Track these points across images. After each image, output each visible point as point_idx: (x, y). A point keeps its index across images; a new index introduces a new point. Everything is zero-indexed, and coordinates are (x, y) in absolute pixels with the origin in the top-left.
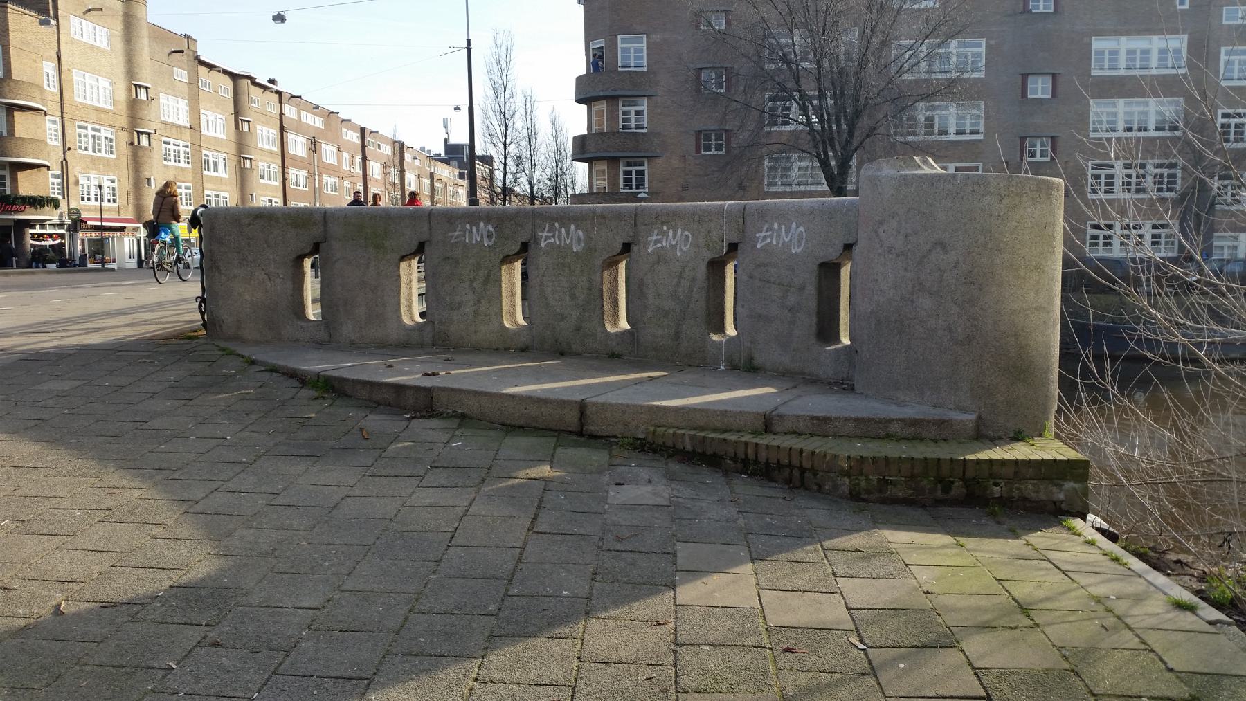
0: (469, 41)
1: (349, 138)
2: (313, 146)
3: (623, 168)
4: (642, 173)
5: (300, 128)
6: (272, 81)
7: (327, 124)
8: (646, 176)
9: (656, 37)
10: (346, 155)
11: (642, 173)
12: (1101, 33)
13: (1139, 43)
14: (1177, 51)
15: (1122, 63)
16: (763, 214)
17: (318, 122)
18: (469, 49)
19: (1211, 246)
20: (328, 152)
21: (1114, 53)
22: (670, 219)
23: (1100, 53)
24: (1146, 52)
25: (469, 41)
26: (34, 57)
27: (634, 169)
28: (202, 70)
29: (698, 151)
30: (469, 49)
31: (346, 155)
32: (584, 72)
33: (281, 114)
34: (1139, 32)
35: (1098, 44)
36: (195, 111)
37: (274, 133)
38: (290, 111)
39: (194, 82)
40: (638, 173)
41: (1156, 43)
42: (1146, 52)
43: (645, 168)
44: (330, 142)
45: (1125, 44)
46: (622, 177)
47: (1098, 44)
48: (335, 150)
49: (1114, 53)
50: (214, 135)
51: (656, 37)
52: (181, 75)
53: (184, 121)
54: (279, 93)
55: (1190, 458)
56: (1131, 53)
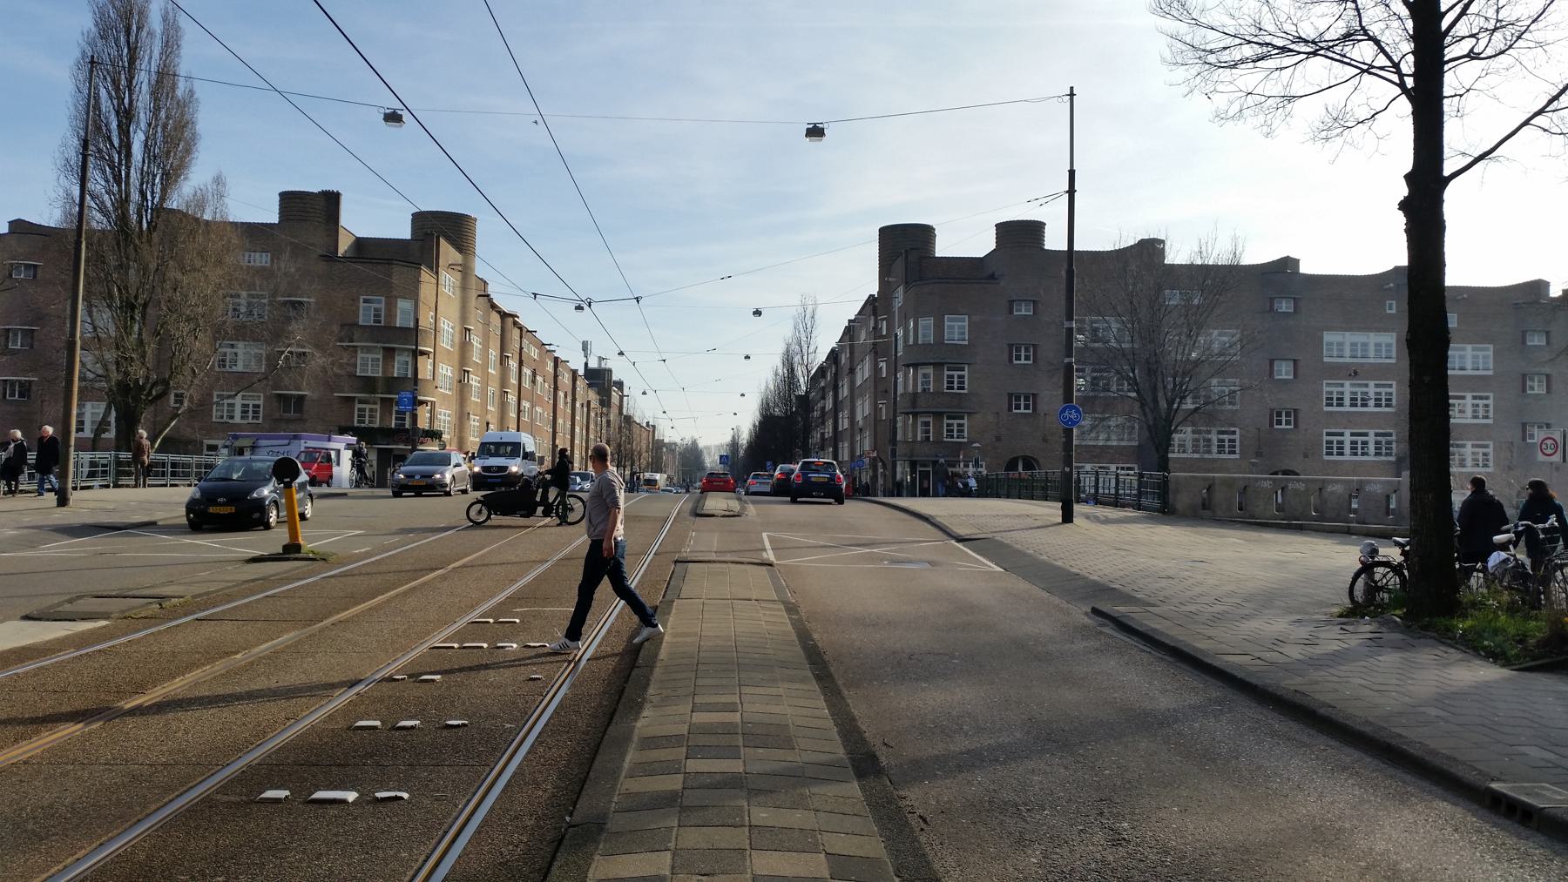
0: (1072, 173)
8: (1359, 409)
9: (976, 318)
12: (1329, 329)
13: (1359, 338)
14: (1389, 345)
15: (1347, 353)
16: (1368, 482)
19: (380, 430)
21: (1340, 344)
22: (1337, 482)
23: (1331, 344)
24: (1365, 345)
25: (1072, 173)
29: (1010, 409)
34: (1360, 329)
35: (1328, 337)
41: (1373, 338)
42: (1365, 345)
43: (965, 422)
45: (1349, 338)
47: (1328, 337)
49: (1340, 344)
51: (976, 318)
56: (1378, 345)
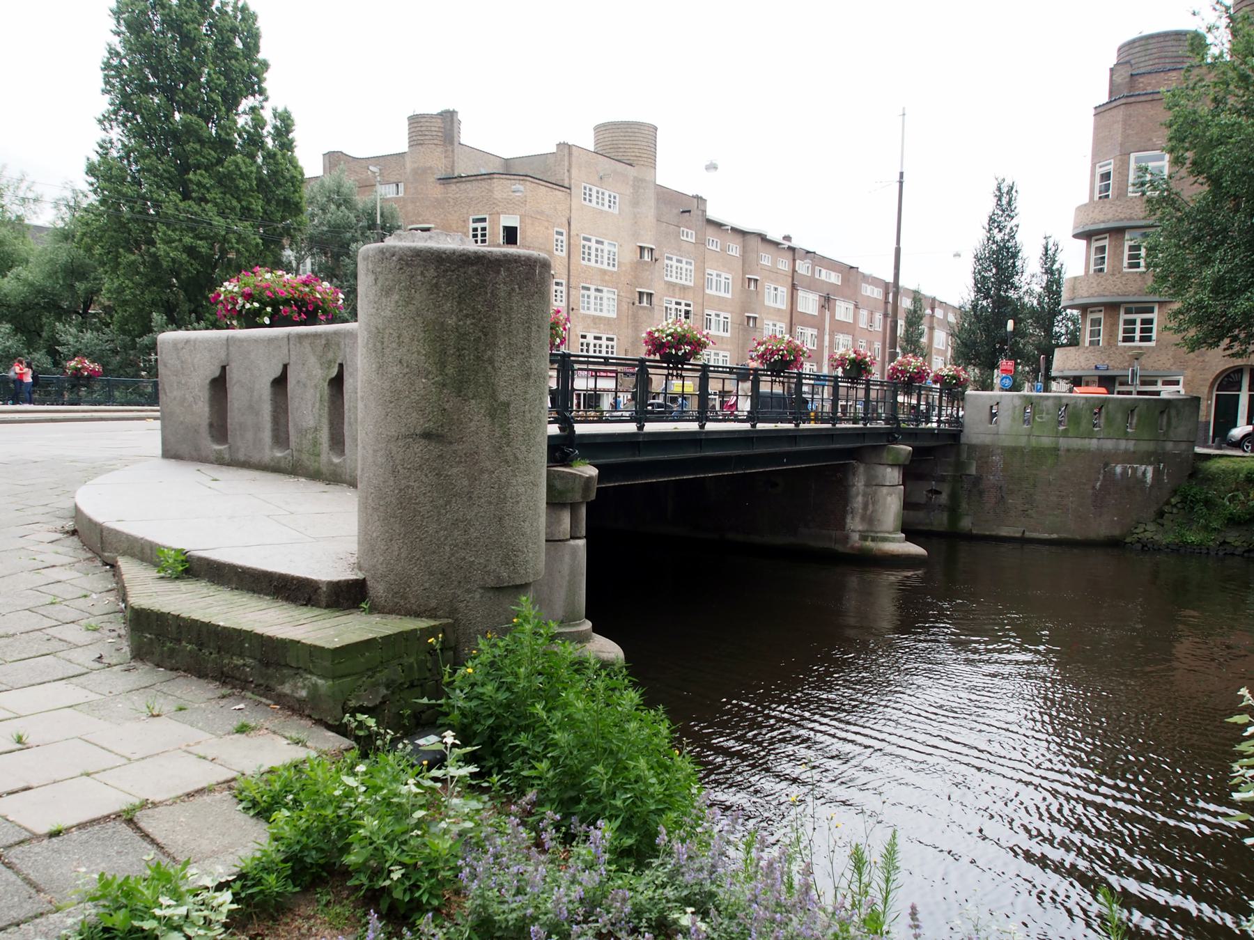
0: (902, 174)
1: (869, 293)
2: (827, 302)
3: (1123, 316)
4: (1150, 321)
5: (812, 285)
6: (787, 238)
7: (845, 280)
8: (1155, 326)
10: (864, 314)
11: (1150, 321)
17: (834, 278)
18: (901, 183)
20: (843, 311)
25: (902, 174)
26: (546, 224)
27: (1139, 317)
28: (710, 230)
30: (901, 183)
31: (864, 314)
32: (1086, 200)
33: (794, 271)
36: (701, 270)
37: (784, 291)
38: (803, 267)
39: (701, 242)
40: (1144, 322)
43: (1154, 316)
44: (846, 298)
46: (1121, 327)
48: (852, 307)
50: (718, 294)
52: (689, 236)
53: (801, 294)
54: (792, 249)
55: (1028, 831)
